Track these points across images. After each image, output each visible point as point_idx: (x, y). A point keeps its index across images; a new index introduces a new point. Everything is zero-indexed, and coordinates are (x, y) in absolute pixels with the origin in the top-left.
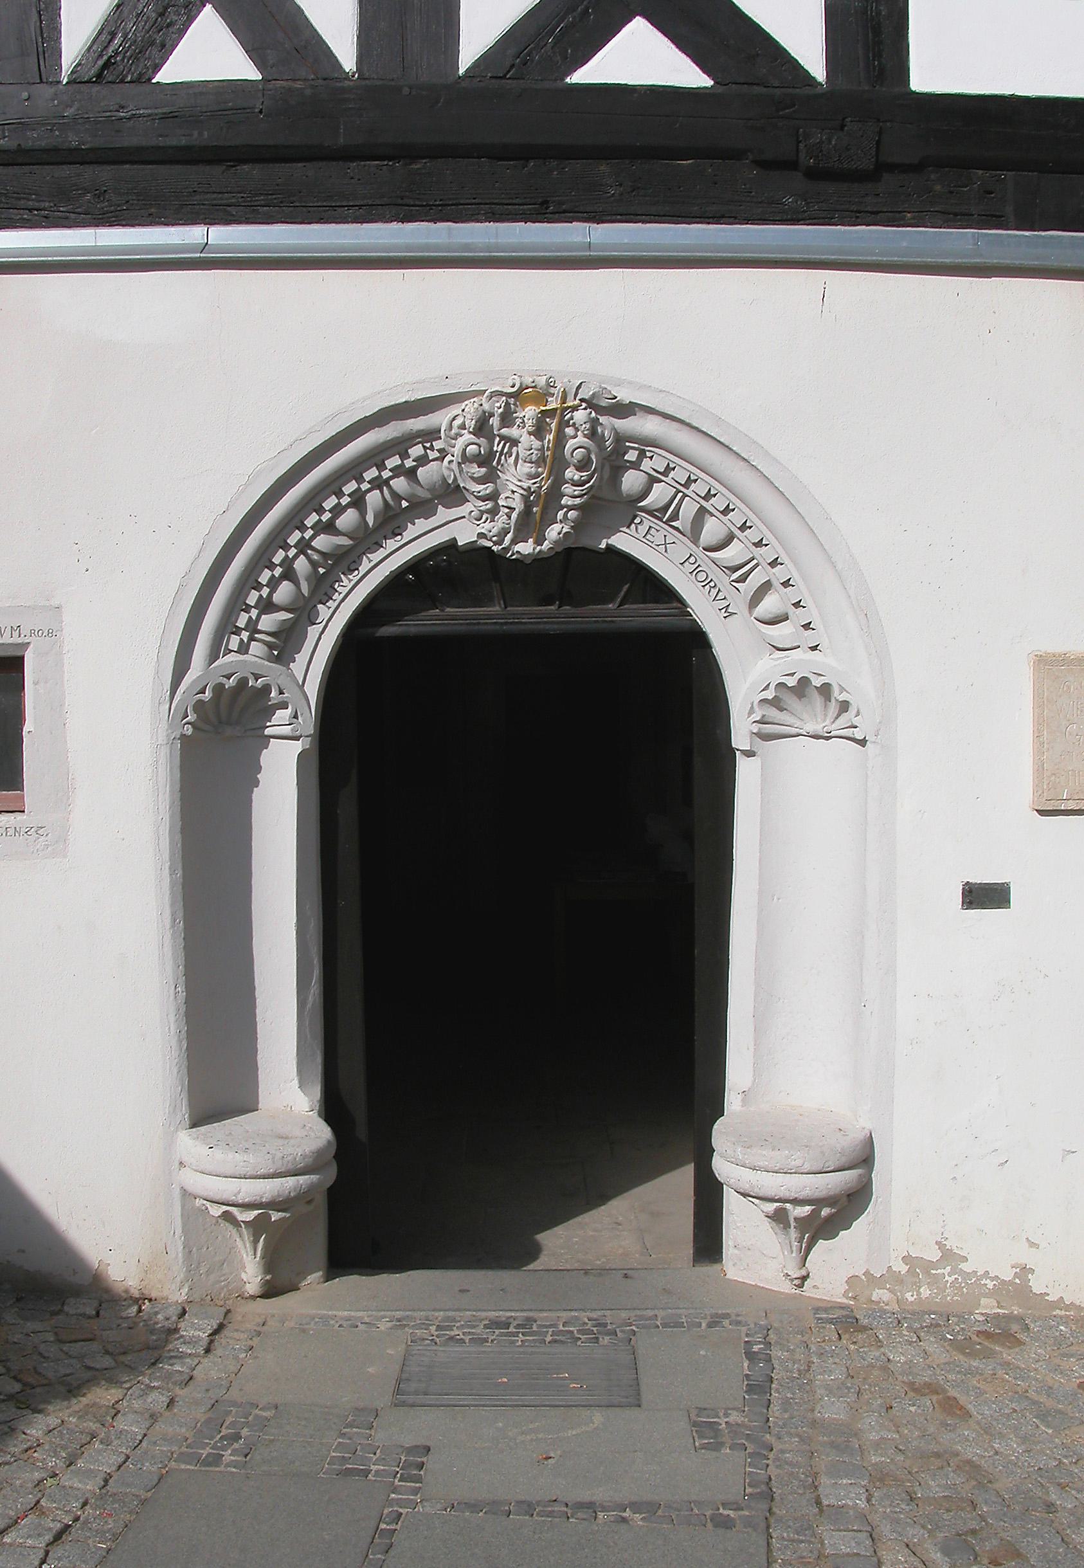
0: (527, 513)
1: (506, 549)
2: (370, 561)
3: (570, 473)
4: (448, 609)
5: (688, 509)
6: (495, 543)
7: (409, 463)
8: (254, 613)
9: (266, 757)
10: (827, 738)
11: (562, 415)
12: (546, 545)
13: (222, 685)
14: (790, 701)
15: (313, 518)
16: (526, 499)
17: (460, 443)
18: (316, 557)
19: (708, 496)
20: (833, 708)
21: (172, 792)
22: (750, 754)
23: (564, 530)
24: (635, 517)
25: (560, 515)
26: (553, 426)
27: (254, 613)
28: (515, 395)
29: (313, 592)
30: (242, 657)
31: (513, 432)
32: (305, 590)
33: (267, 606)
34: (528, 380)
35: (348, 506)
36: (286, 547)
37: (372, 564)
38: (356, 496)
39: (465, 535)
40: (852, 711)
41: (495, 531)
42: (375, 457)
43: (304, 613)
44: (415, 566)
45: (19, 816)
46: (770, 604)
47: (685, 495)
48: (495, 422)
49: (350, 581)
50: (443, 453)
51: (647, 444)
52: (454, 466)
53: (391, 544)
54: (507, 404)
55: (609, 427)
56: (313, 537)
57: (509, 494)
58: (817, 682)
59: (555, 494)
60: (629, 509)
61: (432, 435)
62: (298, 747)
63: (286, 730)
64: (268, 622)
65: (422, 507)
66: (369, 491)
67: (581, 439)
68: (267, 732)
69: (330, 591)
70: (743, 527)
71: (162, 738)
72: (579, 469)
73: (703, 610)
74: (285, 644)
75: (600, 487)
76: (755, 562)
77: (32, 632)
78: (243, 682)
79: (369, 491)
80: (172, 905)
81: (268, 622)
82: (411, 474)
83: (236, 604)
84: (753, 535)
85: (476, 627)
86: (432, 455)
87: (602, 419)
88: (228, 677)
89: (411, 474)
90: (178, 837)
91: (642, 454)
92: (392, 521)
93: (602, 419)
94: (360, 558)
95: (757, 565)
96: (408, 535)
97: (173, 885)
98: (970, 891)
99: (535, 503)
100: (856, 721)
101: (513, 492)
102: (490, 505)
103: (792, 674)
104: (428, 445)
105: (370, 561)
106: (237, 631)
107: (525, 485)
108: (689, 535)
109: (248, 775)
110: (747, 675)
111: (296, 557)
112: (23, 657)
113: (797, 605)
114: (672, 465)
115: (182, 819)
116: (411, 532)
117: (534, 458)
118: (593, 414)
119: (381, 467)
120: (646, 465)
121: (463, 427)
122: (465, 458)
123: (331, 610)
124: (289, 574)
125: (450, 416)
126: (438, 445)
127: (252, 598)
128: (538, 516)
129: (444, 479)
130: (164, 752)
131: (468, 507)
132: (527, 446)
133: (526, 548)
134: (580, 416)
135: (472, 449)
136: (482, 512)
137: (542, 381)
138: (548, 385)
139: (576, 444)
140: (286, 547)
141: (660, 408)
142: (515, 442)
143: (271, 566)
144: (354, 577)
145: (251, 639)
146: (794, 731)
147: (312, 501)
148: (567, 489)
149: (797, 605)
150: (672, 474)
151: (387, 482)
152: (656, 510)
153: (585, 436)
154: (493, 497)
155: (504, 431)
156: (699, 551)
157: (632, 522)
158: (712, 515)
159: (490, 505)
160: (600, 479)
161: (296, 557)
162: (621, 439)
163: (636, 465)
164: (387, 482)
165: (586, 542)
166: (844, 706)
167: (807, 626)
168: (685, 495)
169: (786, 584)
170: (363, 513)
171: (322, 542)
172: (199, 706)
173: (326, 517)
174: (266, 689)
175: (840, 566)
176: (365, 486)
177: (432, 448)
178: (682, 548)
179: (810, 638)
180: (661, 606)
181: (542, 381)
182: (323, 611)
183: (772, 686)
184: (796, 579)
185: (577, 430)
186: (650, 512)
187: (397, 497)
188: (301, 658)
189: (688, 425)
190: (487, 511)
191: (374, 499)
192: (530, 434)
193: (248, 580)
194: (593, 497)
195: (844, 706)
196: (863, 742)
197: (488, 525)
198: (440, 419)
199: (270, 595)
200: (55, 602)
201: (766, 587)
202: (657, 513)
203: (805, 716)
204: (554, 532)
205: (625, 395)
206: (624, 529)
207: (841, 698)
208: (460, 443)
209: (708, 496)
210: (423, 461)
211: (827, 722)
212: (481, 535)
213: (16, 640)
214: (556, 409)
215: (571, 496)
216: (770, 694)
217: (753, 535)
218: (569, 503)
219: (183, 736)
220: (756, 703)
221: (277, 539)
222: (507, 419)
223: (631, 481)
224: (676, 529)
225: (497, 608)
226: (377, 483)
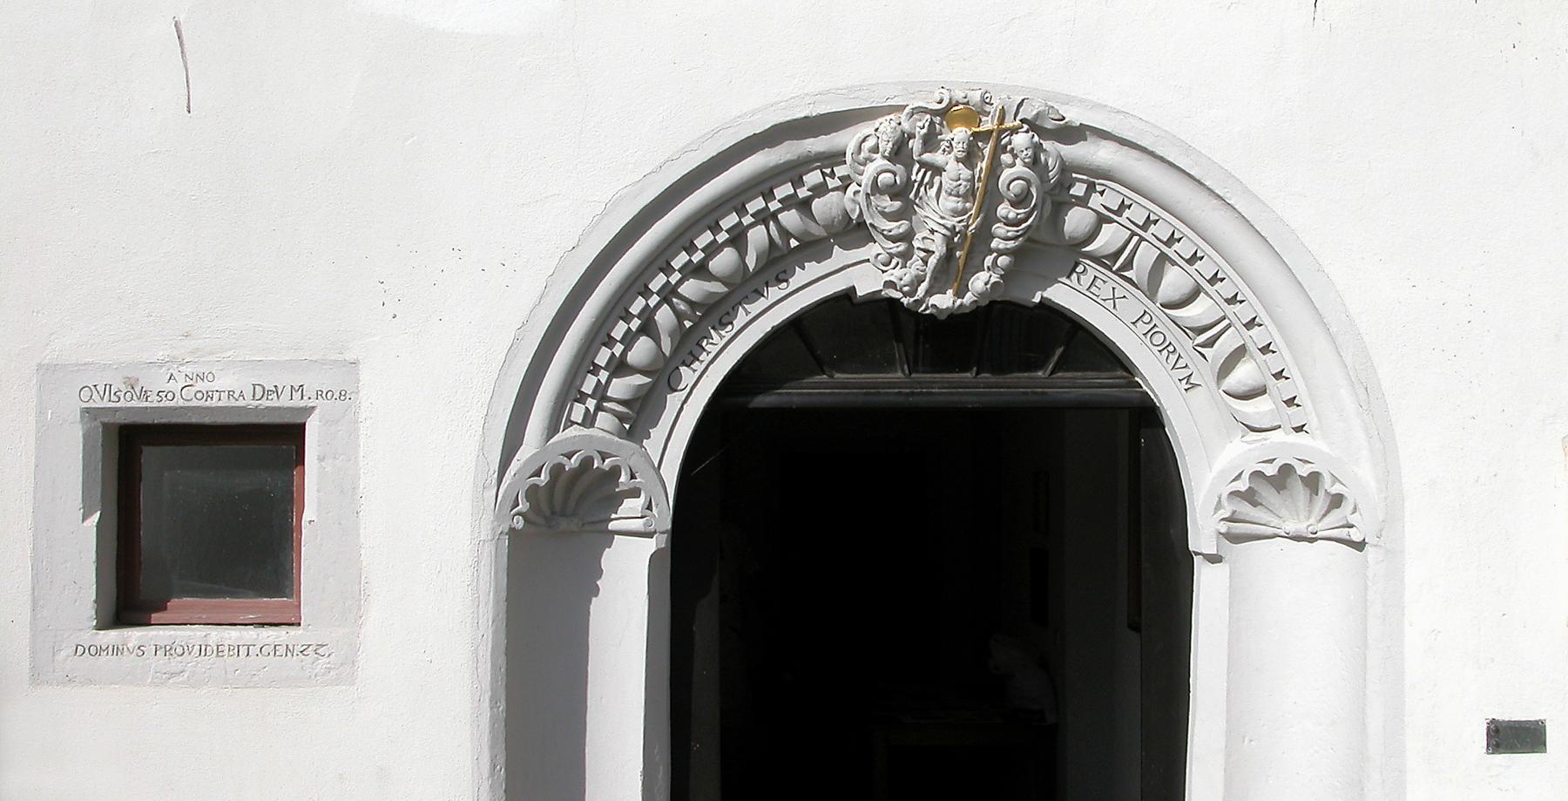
0: (948, 257)
1: (919, 302)
2: (748, 313)
3: (1004, 210)
4: (837, 375)
5: (1146, 256)
6: (905, 295)
7: (803, 193)
8: (604, 376)
9: (609, 559)
10: (1312, 540)
11: (999, 139)
12: (969, 298)
13: (560, 466)
14: (1267, 493)
15: (680, 260)
16: (948, 240)
17: (870, 170)
18: (682, 307)
19: (1171, 241)
20: (1321, 502)
21: (497, 602)
22: (1214, 559)
23: (993, 280)
24: (1077, 264)
25: (988, 261)
26: (987, 152)
27: (604, 376)
28: (943, 113)
29: (675, 351)
30: (586, 431)
31: (937, 158)
32: (667, 347)
33: (620, 367)
34: (959, 95)
35: (727, 243)
36: (646, 293)
37: (750, 317)
38: (736, 232)
39: (867, 282)
40: (1347, 507)
41: (907, 279)
42: (763, 184)
43: (663, 376)
44: (795, 325)
45: (293, 631)
46: (1244, 375)
47: (1142, 239)
48: (915, 145)
49: (722, 337)
50: (846, 182)
51: (1098, 176)
52: (861, 198)
53: (774, 293)
54: (932, 123)
55: (1054, 153)
56: (680, 282)
57: (926, 233)
58: (1303, 470)
59: (984, 235)
60: (1072, 255)
61: (837, 157)
62: (650, 546)
63: (637, 525)
64: (621, 387)
65: (814, 247)
66: (752, 225)
67: (1020, 169)
68: (612, 526)
69: (696, 350)
70: (1214, 280)
71: (486, 533)
72: (1014, 205)
73: (1157, 378)
74: (639, 415)
75: (1038, 227)
76: (1226, 322)
77: (319, 394)
78: (587, 462)
79: (752, 225)
80: (492, 747)
81: (621, 387)
82: (804, 206)
83: (583, 363)
84: (1225, 289)
85: (925, 398)
86: (832, 183)
87: (1047, 145)
88: (569, 456)
89: (804, 206)
90: (502, 660)
91: (1091, 187)
92: (777, 263)
93: (1047, 145)
94: (735, 309)
95: (1229, 326)
96: (795, 282)
97: (493, 721)
98: (1497, 731)
99: (960, 246)
100: (1352, 519)
101: (932, 231)
102: (902, 247)
103: (1271, 461)
104: (828, 171)
105: (748, 313)
106: (582, 398)
107: (949, 224)
108: (1145, 288)
109: (586, 581)
110: (1211, 458)
111: (658, 306)
112: (302, 427)
113: (1279, 375)
114: (1127, 202)
115: (507, 637)
116: (799, 277)
117: (962, 190)
118: (1036, 138)
119: (768, 195)
120: (1096, 201)
121: (875, 149)
122: (876, 188)
123: (697, 374)
124: (648, 327)
125: (860, 135)
126: (840, 171)
127: (602, 358)
128: (961, 262)
129: (846, 214)
130: (489, 549)
131: (870, 250)
132: (953, 175)
133: (944, 301)
134: (1021, 140)
135: (886, 178)
136: (892, 256)
137: (976, 97)
138: (983, 101)
139: (1013, 174)
140: (646, 293)
141: (1117, 132)
142: (938, 170)
143: (627, 317)
144: (727, 333)
145: (599, 408)
146: (1270, 531)
147: (682, 238)
148: (999, 229)
149: (1279, 375)
150: (1127, 213)
151: (774, 216)
152: (1105, 257)
153: (1026, 165)
154: (907, 237)
155: (927, 157)
156: (1155, 309)
157: (1073, 270)
158: (1174, 263)
159: (902, 247)
160: (1040, 217)
161: (658, 306)
162: (1066, 169)
163: (1083, 202)
164: (774, 216)
165: (1017, 295)
166: (1337, 501)
167: (1290, 402)
168: (1142, 239)
169: (1265, 349)
170: (742, 253)
171: (692, 288)
172: (533, 492)
173: (698, 257)
174: (615, 472)
175: (1333, 329)
176: (747, 220)
177: (832, 175)
178: (1134, 303)
179: (1294, 416)
180: (1103, 375)
181: (976, 97)
182: (687, 375)
183: (1246, 476)
184: (1279, 343)
185: (1015, 156)
186: (1097, 259)
187: (786, 234)
188: (658, 433)
189: (1152, 154)
190: (899, 255)
191: (757, 237)
192: (958, 160)
193: (599, 335)
194: (1029, 240)
195: (1337, 501)
196: (1360, 546)
197: (898, 272)
198: (847, 139)
199: (624, 353)
200: (350, 357)
201: (1240, 353)
202: (1105, 260)
203: (1283, 512)
204: (979, 282)
205: (1074, 116)
206: (1064, 280)
207: (1336, 489)
208: (870, 170)
209: (1171, 241)
210: (820, 190)
211: (1312, 520)
212: (890, 284)
213: (297, 402)
214: (990, 132)
215: (1002, 237)
216: (1242, 486)
217: (1225, 289)
218: (1001, 246)
219: (512, 530)
220: (1225, 496)
221: (636, 283)
222: (930, 142)
223: (1076, 221)
224: (1129, 281)
225: (900, 374)
226: (761, 216)
